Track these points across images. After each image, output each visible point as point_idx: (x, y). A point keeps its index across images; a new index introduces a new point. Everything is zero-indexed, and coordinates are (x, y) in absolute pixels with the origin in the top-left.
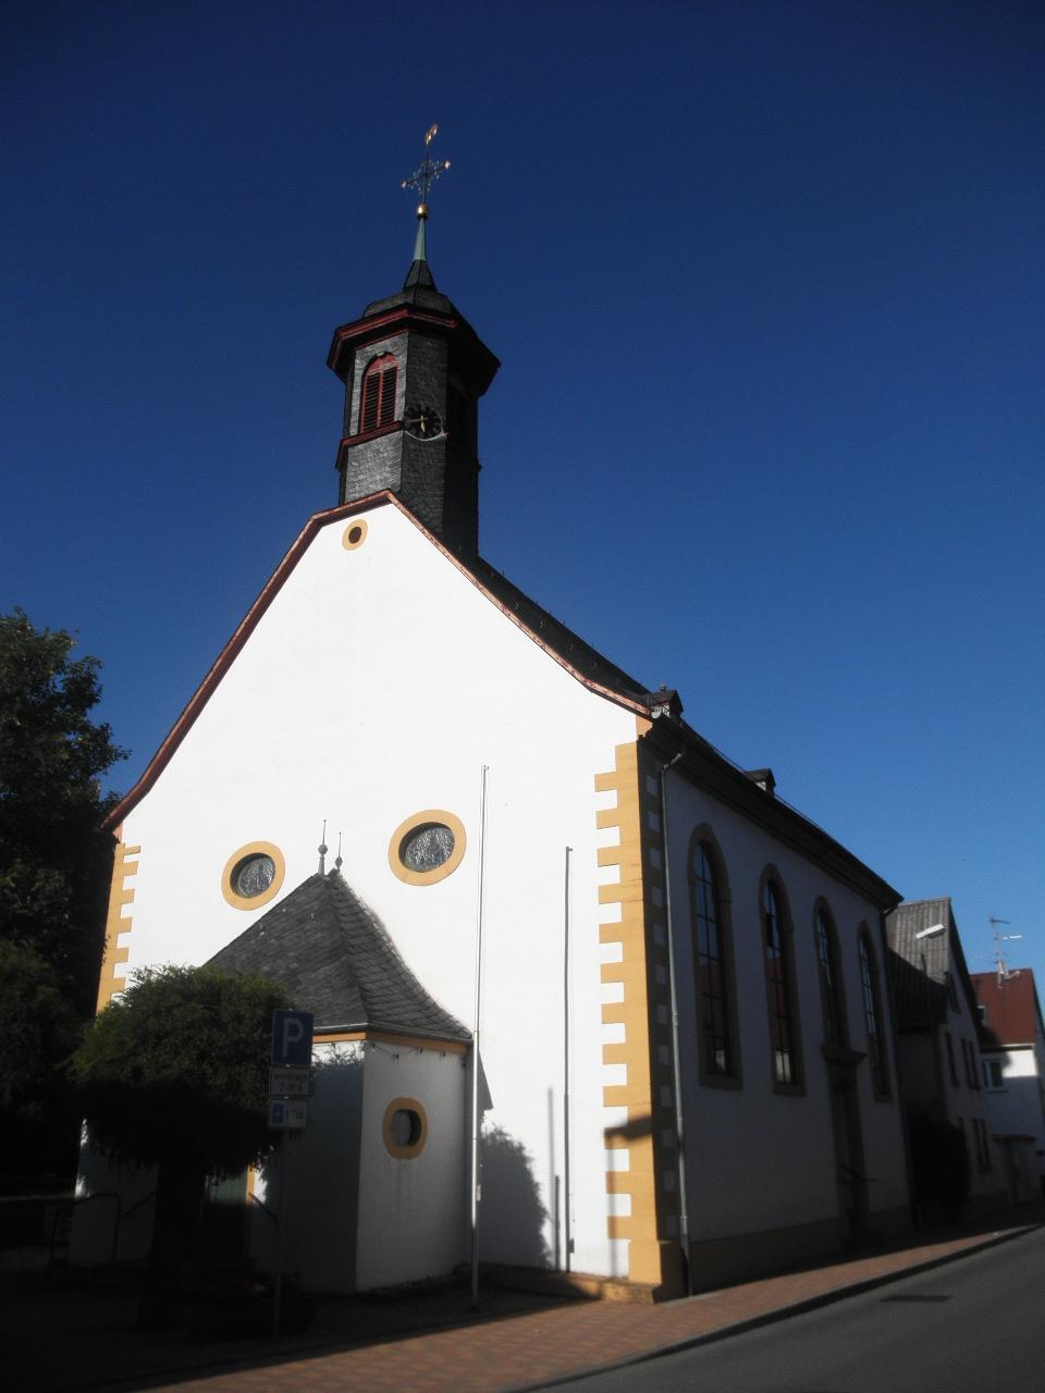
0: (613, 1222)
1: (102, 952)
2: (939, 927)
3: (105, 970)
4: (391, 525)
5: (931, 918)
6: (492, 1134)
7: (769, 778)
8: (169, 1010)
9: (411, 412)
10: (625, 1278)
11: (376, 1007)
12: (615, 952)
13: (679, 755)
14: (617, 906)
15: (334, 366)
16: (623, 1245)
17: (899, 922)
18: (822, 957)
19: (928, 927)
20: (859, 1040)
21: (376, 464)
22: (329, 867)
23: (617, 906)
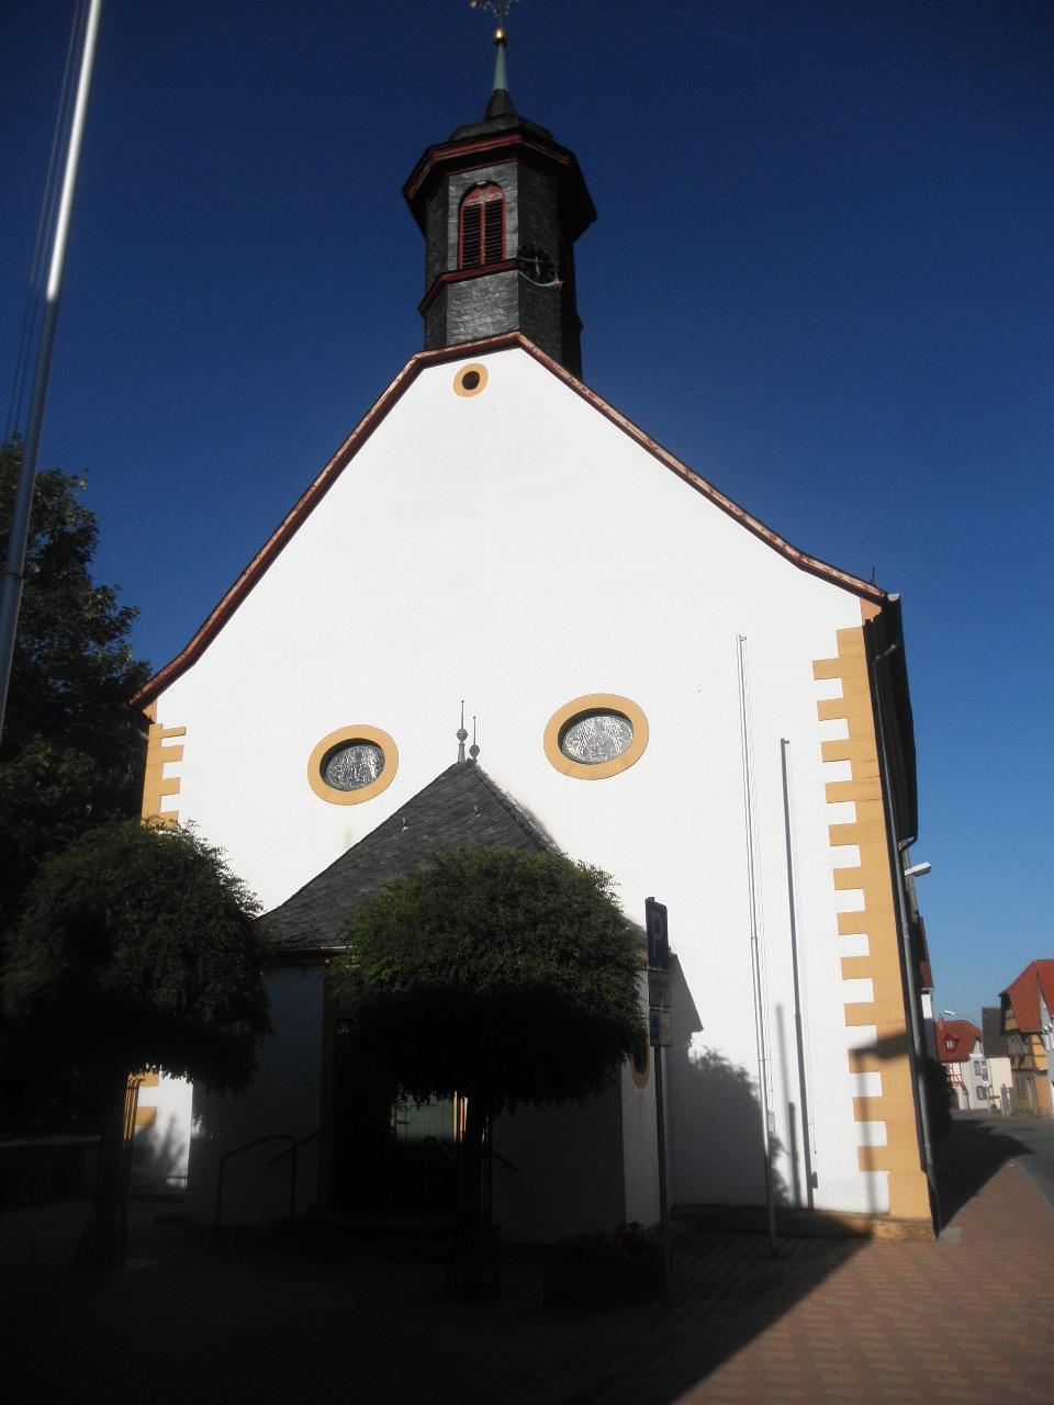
6: (703, 1059)
9: (525, 250)
10: (888, 1214)
14: (851, 806)
16: (881, 1178)
23: (851, 806)
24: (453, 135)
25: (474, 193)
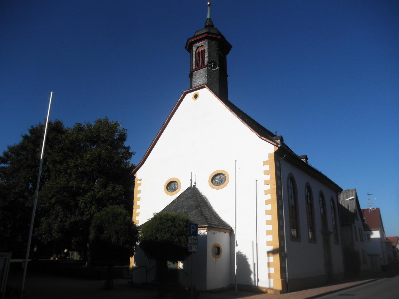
0: (269, 275)
1: (133, 206)
2: (353, 197)
3: (134, 211)
4: (206, 94)
5: (350, 194)
7: (306, 158)
8: (163, 223)
9: (209, 62)
10: (273, 288)
11: (209, 221)
12: (269, 207)
13: (285, 156)
15: (187, 49)
16: (272, 280)
17: (341, 195)
18: (321, 206)
19: (350, 197)
20: (331, 228)
21: (200, 77)
22: (193, 184)
24: (195, 35)
25: (199, 48)
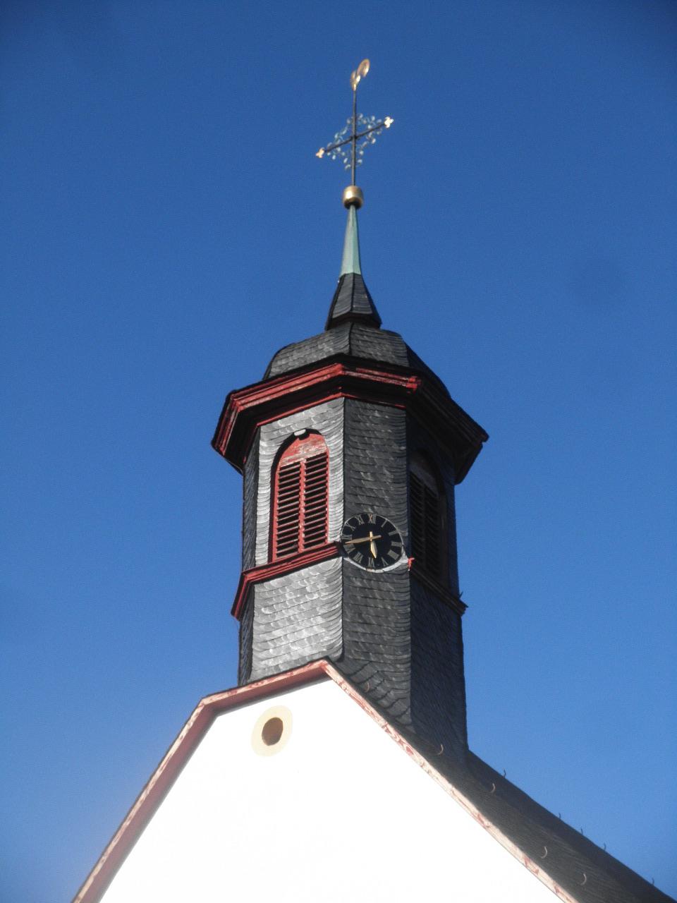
9: (354, 527)
25: (293, 447)
